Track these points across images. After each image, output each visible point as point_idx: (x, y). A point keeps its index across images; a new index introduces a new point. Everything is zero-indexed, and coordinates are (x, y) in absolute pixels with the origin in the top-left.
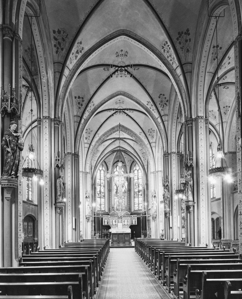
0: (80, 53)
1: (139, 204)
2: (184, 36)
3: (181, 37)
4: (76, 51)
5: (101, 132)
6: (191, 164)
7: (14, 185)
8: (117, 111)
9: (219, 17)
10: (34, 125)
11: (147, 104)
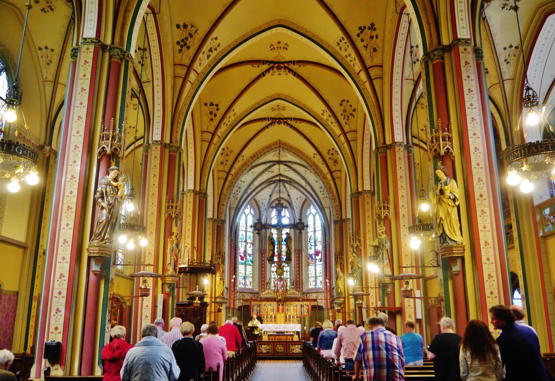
0: (214, 51)
1: (316, 277)
2: (368, 32)
3: (364, 32)
4: (208, 49)
5: (248, 153)
6: (386, 214)
7: (106, 254)
10: (138, 144)
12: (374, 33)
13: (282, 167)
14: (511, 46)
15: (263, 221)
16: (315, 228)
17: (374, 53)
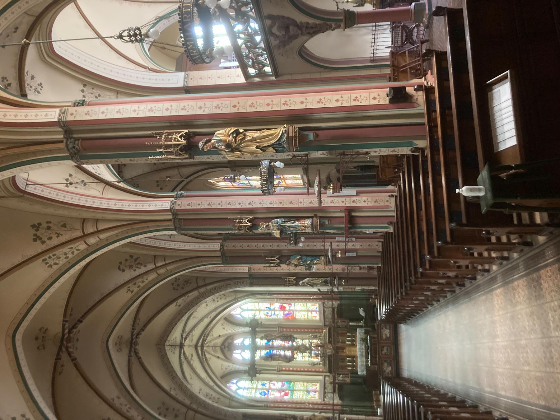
1: (308, 311)
3: (41, 236)
6: (248, 221)
8: (133, 350)
9: (27, 181)
11: (132, 292)
12: (45, 225)
13: (187, 343)
14: (83, 91)
15: (245, 368)
16: (256, 310)
17: (68, 226)
